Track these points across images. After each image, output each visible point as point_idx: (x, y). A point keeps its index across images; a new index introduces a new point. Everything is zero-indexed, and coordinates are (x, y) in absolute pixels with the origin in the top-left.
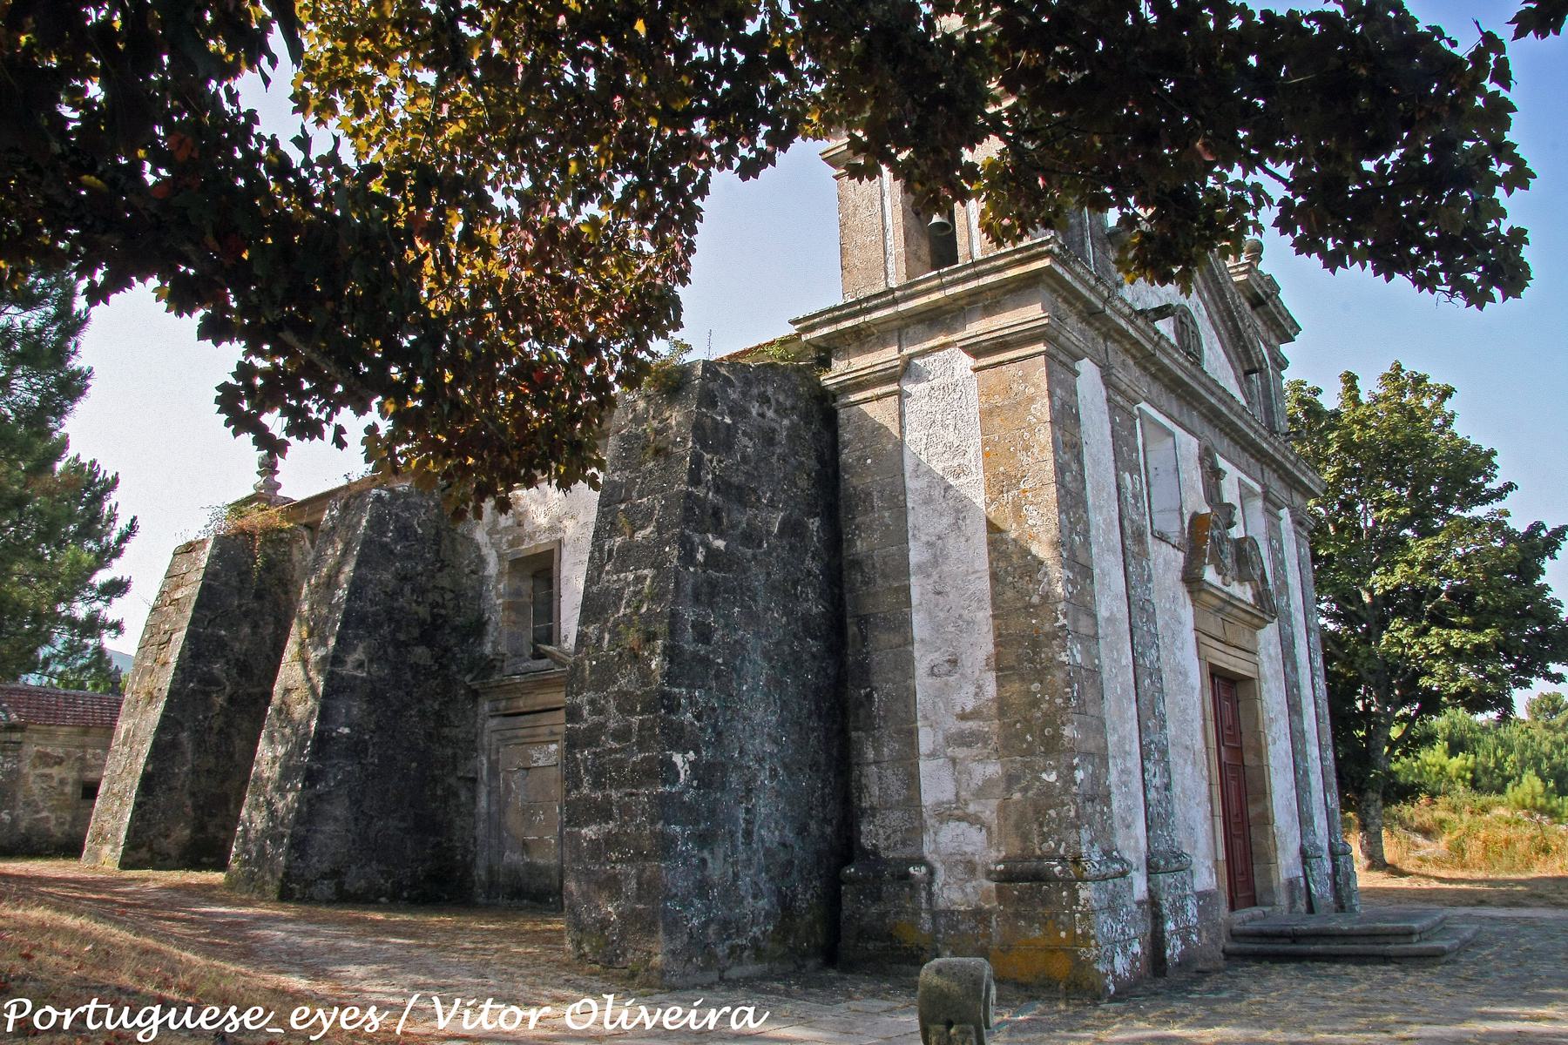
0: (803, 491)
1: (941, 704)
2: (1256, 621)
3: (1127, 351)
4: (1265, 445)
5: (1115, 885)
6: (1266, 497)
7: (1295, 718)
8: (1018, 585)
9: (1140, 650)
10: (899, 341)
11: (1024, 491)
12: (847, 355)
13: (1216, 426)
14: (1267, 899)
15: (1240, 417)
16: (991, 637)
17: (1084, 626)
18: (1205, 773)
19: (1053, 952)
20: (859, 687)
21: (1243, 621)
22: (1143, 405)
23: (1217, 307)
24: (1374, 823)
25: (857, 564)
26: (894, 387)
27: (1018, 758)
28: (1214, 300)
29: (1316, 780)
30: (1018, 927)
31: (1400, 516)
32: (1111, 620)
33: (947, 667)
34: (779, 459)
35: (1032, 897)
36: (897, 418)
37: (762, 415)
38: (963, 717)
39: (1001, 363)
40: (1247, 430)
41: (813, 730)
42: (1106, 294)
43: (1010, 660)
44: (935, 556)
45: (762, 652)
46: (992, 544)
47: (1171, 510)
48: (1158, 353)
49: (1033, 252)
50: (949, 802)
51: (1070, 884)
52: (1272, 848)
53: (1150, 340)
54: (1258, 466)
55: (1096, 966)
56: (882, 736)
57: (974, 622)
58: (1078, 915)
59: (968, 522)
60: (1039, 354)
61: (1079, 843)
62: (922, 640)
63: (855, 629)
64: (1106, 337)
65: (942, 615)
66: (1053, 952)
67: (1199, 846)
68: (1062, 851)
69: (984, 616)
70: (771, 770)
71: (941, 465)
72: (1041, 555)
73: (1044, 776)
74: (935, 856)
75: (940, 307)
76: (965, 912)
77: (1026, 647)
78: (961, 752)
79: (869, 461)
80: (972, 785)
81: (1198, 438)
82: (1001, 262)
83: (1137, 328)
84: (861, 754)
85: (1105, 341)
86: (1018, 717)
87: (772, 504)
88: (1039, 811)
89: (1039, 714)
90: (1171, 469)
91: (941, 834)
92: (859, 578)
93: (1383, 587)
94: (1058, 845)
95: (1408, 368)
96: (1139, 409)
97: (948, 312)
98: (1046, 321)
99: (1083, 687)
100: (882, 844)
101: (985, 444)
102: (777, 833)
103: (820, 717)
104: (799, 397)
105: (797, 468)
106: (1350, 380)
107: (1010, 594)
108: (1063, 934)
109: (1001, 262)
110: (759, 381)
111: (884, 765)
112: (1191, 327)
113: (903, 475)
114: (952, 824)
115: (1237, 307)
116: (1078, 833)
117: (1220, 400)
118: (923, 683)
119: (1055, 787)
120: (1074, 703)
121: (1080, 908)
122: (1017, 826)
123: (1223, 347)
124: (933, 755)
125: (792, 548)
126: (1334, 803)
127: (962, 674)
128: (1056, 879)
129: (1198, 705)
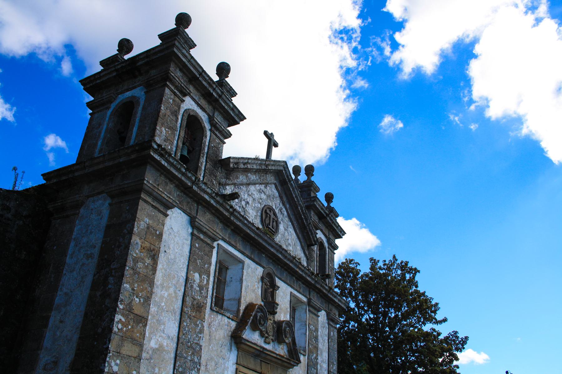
2: (286, 364)
15: (292, 262)
21: (276, 363)
22: (221, 243)
32: (160, 350)
42: (194, 178)
53: (227, 210)
79: (55, 247)
81: (263, 267)
83: (217, 202)
85: (198, 205)
90: (239, 279)
96: (218, 244)
112: (272, 216)
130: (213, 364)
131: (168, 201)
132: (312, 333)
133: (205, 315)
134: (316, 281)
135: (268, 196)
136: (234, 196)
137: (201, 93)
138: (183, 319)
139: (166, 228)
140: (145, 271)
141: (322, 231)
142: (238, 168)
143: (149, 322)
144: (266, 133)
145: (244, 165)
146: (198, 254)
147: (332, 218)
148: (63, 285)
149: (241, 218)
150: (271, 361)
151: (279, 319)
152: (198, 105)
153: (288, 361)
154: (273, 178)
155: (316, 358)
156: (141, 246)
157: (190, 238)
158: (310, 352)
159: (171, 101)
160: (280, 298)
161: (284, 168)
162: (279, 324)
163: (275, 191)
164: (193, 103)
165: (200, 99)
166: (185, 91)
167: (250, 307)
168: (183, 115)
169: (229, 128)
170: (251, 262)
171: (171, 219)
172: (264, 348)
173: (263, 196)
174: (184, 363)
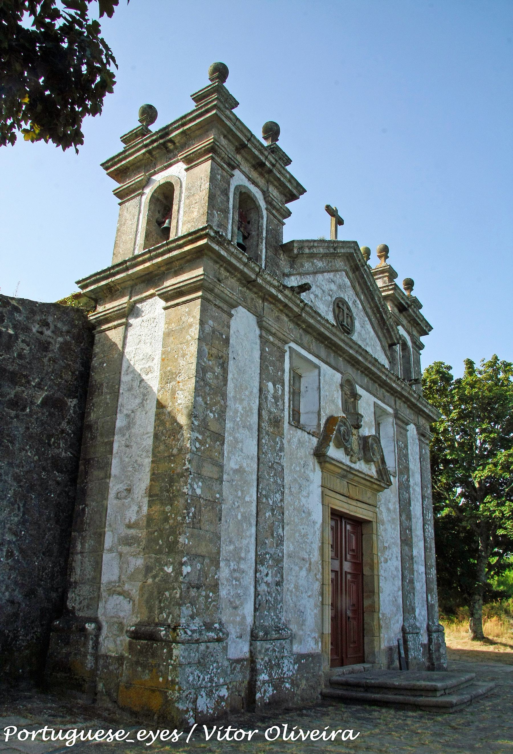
0: (66, 381)
1: (119, 518)
2: (375, 486)
3: (281, 311)
4: (394, 385)
5: (208, 647)
6: (396, 416)
7: (406, 548)
8: (167, 442)
9: (264, 493)
10: (131, 293)
11: (179, 382)
12: (105, 303)
13: (358, 369)
14: (370, 659)
15: (373, 365)
16: (149, 475)
17: (208, 470)
18: (319, 576)
19: (153, 691)
20: (79, 505)
22: (293, 345)
23: (370, 305)
24: (477, 613)
25: (90, 427)
26: (124, 320)
27: (153, 555)
28: (368, 300)
29: (420, 586)
30: (136, 671)
31: (491, 438)
32: (240, 471)
33: (125, 493)
34: (49, 360)
35: (146, 652)
36: (122, 339)
37: (41, 333)
38: (129, 526)
39: (178, 304)
40: (381, 375)
41: (50, 529)
42: (257, 269)
43: (156, 491)
44: (129, 423)
45: (13, 476)
46: (157, 415)
47: (313, 413)
48: (303, 315)
49: (198, 235)
50: (115, 582)
51: (168, 644)
52: (376, 627)
53: (298, 306)
54: (393, 398)
55: (176, 705)
56: (86, 536)
57: (142, 465)
58: (170, 667)
59: (148, 401)
60: (198, 298)
61: (179, 616)
62: (115, 476)
63: (83, 467)
64: (264, 299)
65: (127, 460)
66: (153, 691)
67: (307, 623)
68: (169, 621)
69: (147, 461)
70: (8, 551)
71: (141, 367)
72: (181, 423)
73: (166, 568)
74: (104, 618)
75: (151, 272)
76: (115, 657)
77: (166, 482)
78: (125, 549)
79: (105, 365)
80: (129, 572)
81: (341, 373)
82: (181, 242)
83: (286, 296)
84: (75, 547)
85: (263, 302)
86: (156, 528)
87: (39, 386)
88: (161, 593)
89: (167, 527)
91: (109, 603)
92: (89, 435)
93: (480, 477)
94: (168, 616)
95: (501, 359)
96: (290, 347)
97: (157, 275)
98: (202, 277)
99: (200, 511)
100: (77, 607)
101: (163, 353)
102: (7, 594)
103: (57, 522)
104: (74, 326)
105: (64, 368)
106: (470, 364)
107: (162, 447)
108: (161, 679)
109: (181, 242)
110: (42, 312)
111: (85, 555)
112: (346, 311)
113: (120, 373)
114: (115, 597)
115: (382, 306)
116: (180, 609)
117: (357, 352)
118: (112, 502)
119: (171, 576)
120: (188, 520)
121: (172, 662)
122: (147, 602)
123: (373, 328)
124: (110, 550)
125: (51, 415)
126: (434, 600)
127: (132, 498)
128: (161, 640)
129: (318, 533)
130: (297, 486)
131: (231, 298)
132: (401, 450)
133: (283, 431)
134: (402, 388)
135: (340, 287)
136: (305, 288)
137: (251, 163)
138: (261, 436)
139: (232, 332)
140: (215, 381)
141: (403, 326)
142: (303, 254)
143: (226, 440)
144: (328, 209)
145: (309, 249)
146: (269, 360)
147: (415, 310)
148: (122, 405)
149: (313, 314)
150: (359, 483)
151: (364, 434)
152: (249, 179)
153: (378, 483)
154: (342, 263)
155: (408, 480)
156: (209, 353)
157: (258, 341)
158: (401, 473)
159: (219, 177)
160: (362, 410)
161: (355, 250)
162: (365, 439)
163: (347, 280)
164: (244, 177)
165: (250, 171)
166: (233, 163)
167: (331, 420)
168: (235, 194)
169: (286, 205)
170: (327, 366)
171: (235, 319)
172: (351, 468)
173: (333, 287)
174: (267, 485)
